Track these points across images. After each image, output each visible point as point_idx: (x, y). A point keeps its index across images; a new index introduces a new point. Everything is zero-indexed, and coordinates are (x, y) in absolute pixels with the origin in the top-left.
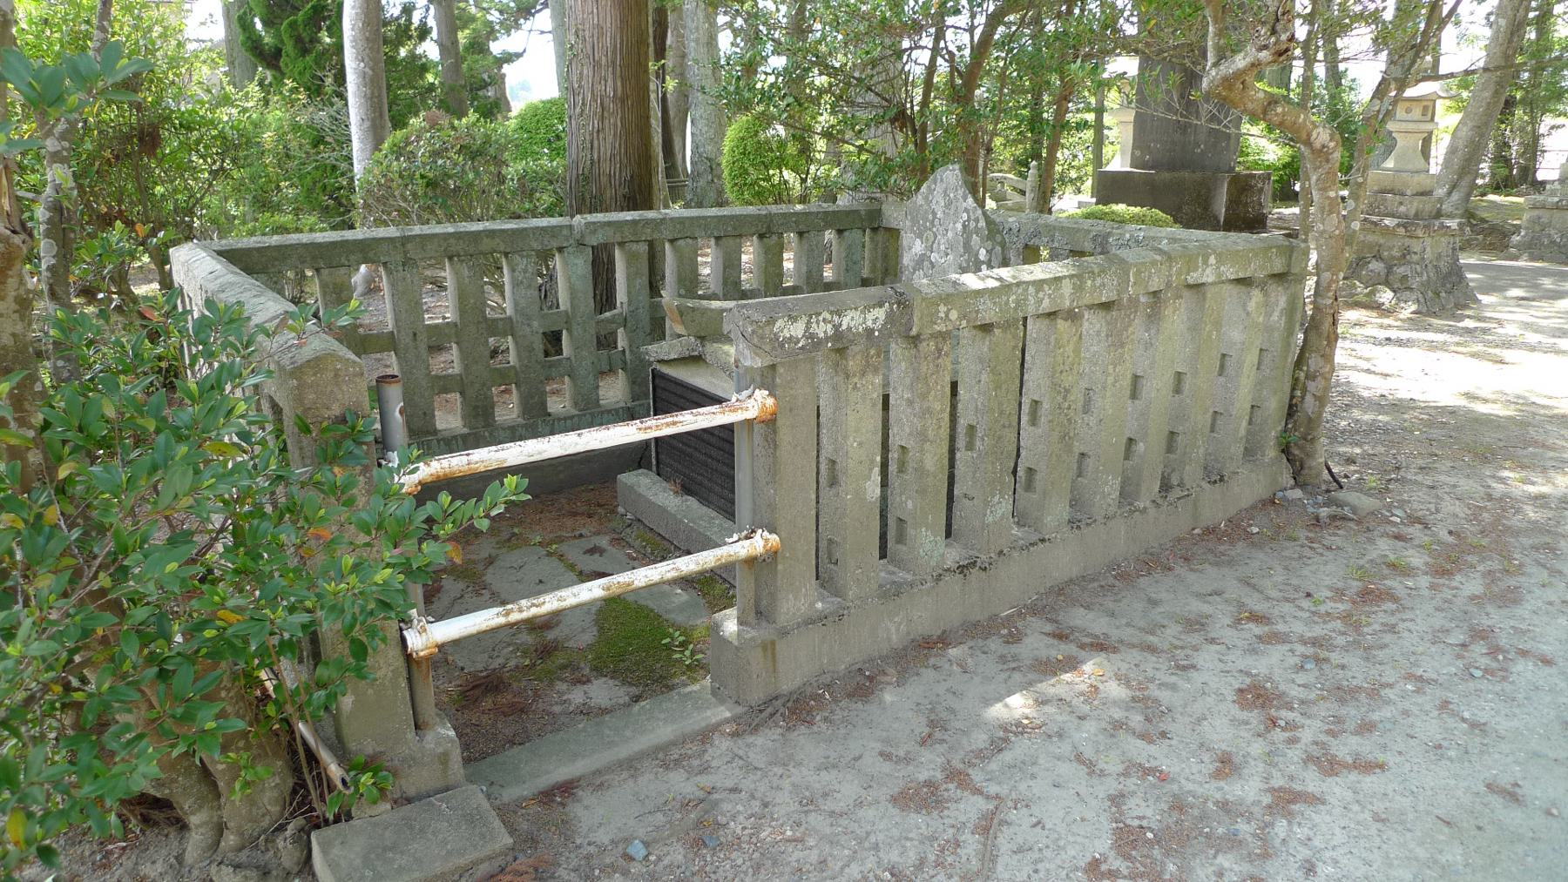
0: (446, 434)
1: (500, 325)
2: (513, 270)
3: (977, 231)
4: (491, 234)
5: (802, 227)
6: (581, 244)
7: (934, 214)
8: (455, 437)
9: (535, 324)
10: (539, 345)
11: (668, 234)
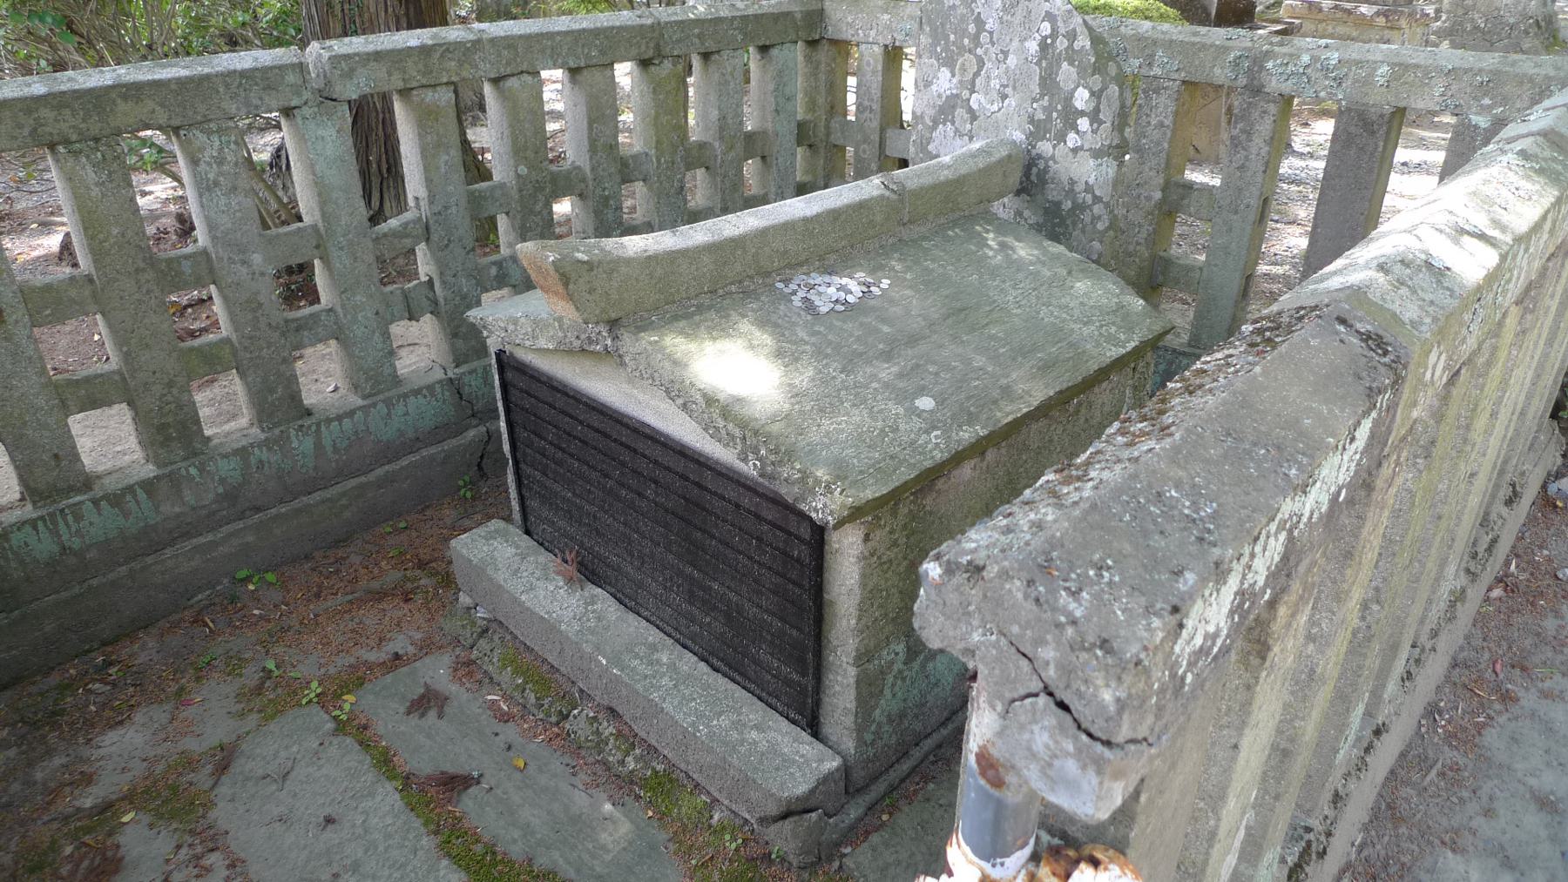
0: (111, 484)
1: (186, 267)
2: (194, 162)
3: (1071, 56)
4: (133, 91)
5: (710, 45)
6: (327, 98)
7: (980, 23)
8: (130, 489)
9: (257, 258)
10: (269, 293)
11: (487, 69)
